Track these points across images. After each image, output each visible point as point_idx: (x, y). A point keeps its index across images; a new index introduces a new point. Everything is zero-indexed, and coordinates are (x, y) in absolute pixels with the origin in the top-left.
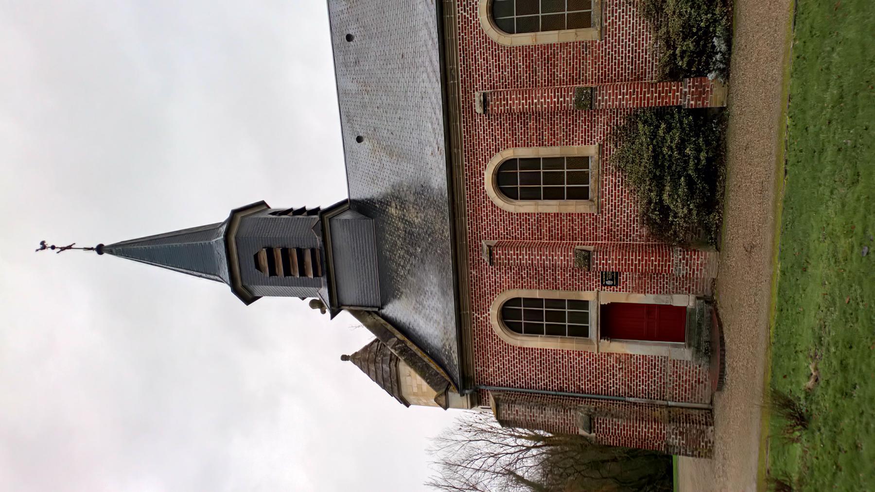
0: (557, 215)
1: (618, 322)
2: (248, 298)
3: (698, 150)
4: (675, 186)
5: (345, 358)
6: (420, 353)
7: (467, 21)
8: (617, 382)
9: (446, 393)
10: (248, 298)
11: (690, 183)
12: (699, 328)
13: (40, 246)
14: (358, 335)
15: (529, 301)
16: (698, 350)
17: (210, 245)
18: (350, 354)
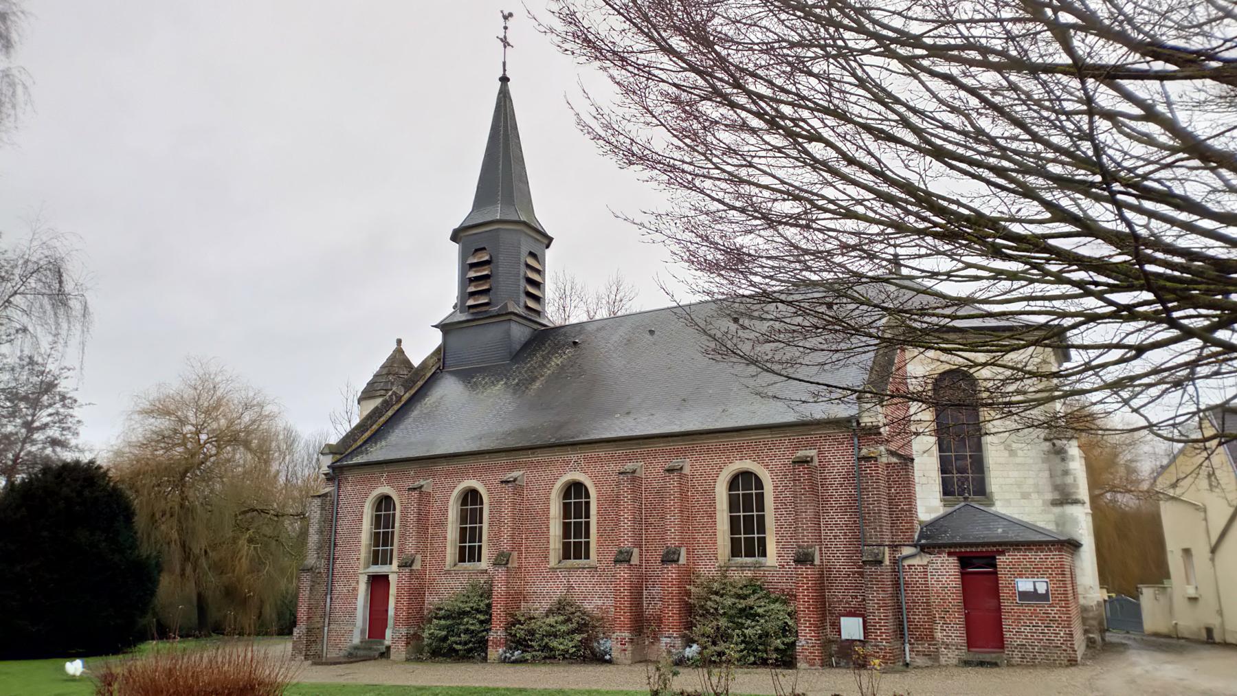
0: (445, 538)
1: (378, 583)
3: (466, 643)
5: (399, 342)
6: (383, 419)
8: (340, 588)
10: (455, 236)
11: (445, 639)
12: (372, 649)
13: (506, 13)
15: (761, 497)
16: (356, 648)
18: (403, 346)
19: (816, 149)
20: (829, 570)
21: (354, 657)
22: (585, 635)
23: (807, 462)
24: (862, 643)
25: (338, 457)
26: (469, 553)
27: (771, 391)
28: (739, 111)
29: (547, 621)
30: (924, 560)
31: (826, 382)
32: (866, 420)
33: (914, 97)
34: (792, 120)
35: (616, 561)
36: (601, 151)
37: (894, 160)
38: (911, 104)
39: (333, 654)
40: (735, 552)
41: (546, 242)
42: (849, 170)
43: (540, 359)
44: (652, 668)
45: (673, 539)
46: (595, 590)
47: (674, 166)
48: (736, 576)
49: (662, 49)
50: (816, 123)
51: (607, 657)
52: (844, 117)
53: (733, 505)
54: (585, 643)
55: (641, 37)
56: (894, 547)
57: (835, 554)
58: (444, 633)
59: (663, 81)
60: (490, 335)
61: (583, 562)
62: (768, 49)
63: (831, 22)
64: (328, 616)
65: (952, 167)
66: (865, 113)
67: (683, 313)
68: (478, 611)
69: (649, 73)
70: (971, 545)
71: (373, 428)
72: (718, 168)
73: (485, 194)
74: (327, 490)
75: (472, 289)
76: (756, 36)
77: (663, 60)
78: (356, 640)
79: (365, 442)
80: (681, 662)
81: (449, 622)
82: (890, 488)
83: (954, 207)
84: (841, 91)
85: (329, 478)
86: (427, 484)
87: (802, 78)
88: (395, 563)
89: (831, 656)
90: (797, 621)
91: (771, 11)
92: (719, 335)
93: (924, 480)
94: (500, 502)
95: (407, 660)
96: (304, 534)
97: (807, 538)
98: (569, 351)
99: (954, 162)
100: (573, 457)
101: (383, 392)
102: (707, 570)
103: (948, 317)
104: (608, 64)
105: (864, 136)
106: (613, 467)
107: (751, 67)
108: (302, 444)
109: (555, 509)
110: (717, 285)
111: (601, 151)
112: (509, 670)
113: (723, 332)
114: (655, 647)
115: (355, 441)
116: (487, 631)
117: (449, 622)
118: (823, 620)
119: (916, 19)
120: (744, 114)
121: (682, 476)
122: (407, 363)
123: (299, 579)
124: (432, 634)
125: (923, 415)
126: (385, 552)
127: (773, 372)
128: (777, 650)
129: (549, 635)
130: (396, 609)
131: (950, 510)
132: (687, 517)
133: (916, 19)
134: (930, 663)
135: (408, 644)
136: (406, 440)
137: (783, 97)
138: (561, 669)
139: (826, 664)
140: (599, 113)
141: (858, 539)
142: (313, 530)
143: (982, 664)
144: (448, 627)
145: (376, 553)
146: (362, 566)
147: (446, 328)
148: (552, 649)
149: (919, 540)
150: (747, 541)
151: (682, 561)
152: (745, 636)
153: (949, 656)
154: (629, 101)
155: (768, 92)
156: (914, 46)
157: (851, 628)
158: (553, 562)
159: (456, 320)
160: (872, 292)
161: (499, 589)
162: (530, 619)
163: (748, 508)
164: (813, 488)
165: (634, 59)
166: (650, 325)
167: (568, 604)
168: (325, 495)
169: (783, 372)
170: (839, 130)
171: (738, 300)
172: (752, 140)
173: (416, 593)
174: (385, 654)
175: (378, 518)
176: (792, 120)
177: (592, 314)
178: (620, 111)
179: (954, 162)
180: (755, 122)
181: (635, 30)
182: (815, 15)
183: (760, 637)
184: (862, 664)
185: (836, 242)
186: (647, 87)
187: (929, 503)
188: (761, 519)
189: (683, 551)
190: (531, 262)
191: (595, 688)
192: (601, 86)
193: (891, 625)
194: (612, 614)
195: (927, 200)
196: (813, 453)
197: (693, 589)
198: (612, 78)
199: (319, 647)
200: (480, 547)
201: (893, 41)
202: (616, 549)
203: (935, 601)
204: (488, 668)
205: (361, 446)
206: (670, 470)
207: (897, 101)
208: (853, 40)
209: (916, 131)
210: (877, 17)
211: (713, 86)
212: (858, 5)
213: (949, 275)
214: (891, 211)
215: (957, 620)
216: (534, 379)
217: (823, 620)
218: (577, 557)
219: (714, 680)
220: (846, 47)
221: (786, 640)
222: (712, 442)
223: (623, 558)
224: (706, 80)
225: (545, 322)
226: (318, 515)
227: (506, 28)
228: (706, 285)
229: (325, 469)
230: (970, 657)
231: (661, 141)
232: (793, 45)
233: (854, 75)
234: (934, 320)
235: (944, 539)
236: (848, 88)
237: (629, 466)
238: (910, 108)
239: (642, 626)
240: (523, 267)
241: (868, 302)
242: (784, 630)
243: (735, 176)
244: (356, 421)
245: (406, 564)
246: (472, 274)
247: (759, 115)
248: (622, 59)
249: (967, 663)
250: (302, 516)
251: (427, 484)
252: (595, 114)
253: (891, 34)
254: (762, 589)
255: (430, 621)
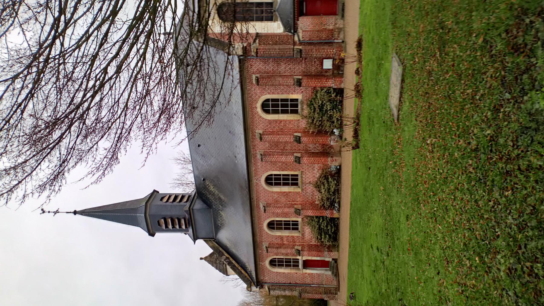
1: (307, 264)
2: (152, 235)
3: (332, 227)
4: (325, 237)
5: (201, 259)
6: (236, 265)
7: (257, 183)
8: (308, 281)
9: (251, 287)
10: (152, 235)
11: (330, 236)
12: (333, 266)
13: (42, 212)
14: (204, 248)
15: (273, 100)
16: (333, 273)
17: (136, 216)
19: (111, 70)
20: (304, 72)
21: (336, 274)
22: (329, 176)
23: (258, 79)
24: (334, 60)
25: (252, 284)
26: (295, 226)
27: (227, 96)
28: (91, 106)
29: (323, 192)
30: (300, 31)
31: (223, 70)
32: (240, 52)
33: (86, 23)
34: (96, 81)
35: (299, 163)
36: (110, 173)
37: (116, 35)
38: (89, 25)
39: (335, 283)
40: (296, 112)
41: (156, 193)
42: (122, 55)
43: (210, 196)
44: (343, 149)
45: (289, 139)
46: (310, 172)
47: (119, 137)
48: (306, 112)
49: (59, 141)
50: (98, 71)
51: (338, 167)
52: (95, 57)
53: (276, 112)
54: (332, 176)
55: (53, 152)
56: (294, 44)
57: (298, 69)
58: (327, 236)
59: (75, 142)
60: (199, 218)
61: (299, 177)
62: (60, 91)
63: (46, 61)
64: (319, 285)
65: (121, 7)
66: (94, 46)
67: (191, 135)
68: (319, 222)
69: (71, 149)
70: (294, 11)
71: (240, 268)
72: (119, 117)
73: (131, 221)
74: (266, 288)
75: (177, 227)
76: (53, 97)
77: (64, 143)
78: (330, 273)
79: (247, 272)
80: (341, 137)
81: (323, 234)
82: (269, 44)
83: (140, 9)
84: (82, 57)
85: (262, 287)
86: (265, 245)
87: (75, 75)
88: (298, 257)
89: (339, 74)
90: (325, 87)
91: (40, 89)
92: (202, 119)
93: (266, 29)
94: (273, 213)
95: (338, 251)
96: (285, 297)
97: (291, 81)
98: (207, 183)
99: (119, 6)
100: (254, 181)
101: (224, 265)
102: (303, 124)
103: (193, 14)
104: (66, 169)
105: (106, 47)
106: (259, 164)
107: (69, 100)
108: (246, 299)
109: (276, 189)
110: (178, 118)
111: (110, 173)
112: (342, 209)
113: (199, 113)
114: (334, 147)
115: (246, 277)
116: (327, 217)
117: (323, 234)
118: (324, 76)
119: (45, 20)
120: (93, 104)
121: (263, 134)
122: (211, 255)
123: (304, 299)
124: (328, 241)
125: (240, 27)
126: (293, 262)
127: (219, 95)
128: (336, 96)
129: (329, 192)
130: (317, 256)
131: (279, 19)
132: (281, 132)
133: (45, 20)
134: (342, 32)
135: (331, 251)
136: (246, 255)
137: (84, 86)
138: (343, 187)
139: (342, 76)
140: (92, 173)
141: (291, 59)
142: (283, 293)
143: (343, 10)
144: (325, 235)
145: (294, 266)
146: (299, 272)
147: (195, 238)
148: (335, 190)
149: (291, 33)
150: (290, 106)
151: (299, 135)
152: (330, 110)
153: (340, 23)
154: (85, 158)
155: (81, 94)
156: (59, 21)
157: (328, 64)
158: (299, 190)
159: (192, 234)
160: (181, 48)
161: (310, 213)
162: (322, 200)
163: (277, 106)
164: (269, 77)
165: (64, 157)
166: (196, 146)
167: (317, 184)
168: (269, 289)
169: (219, 90)
170: (102, 58)
171: (185, 109)
172: (106, 100)
173: (311, 248)
174: (335, 260)
175: (279, 265)
176: (96, 81)
177: (190, 171)
178: (90, 163)
179: (119, 6)
180: (97, 98)
181: (49, 156)
182: (43, 68)
183: (331, 103)
184: (343, 60)
185: (158, 64)
186: (78, 150)
187: (275, 27)
188: (282, 100)
189: (296, 134)
190: (165, 200)
191: (350, 173)
192: (77, 173)
193: (326, 47)
194: (322, 166)
195: (138, 19)
196: (254, 77)
197: (311, 131)
198: (73, 167)
199: (332, 289)
200: (292, 221)
201: (56, 31)
202: (295, 163)
203: (317, 28)
204: (342, 217)
205: (248, 274)
206: (261, 139)
207: (88, 31)
208: (56, 51)
209: (103, 22)
210: (44, 39)
211: (79, 119)
212: (38, 47)
213: (174, 12)
214: (142, 38)
215: (325, 18)
216: (220, 199)
217: (324, 76)
218: (297, 179)
219: (348, 123)
220: (59, 55)
221: (332, 92)
222: (249, 121)
223: (298, 160)
224: (76, 121)
225: (193, 193)
226: (277, 292)
227: (49, 212)
228: (178, 124)
229: (258, 289)
230: (340, 14)
231: (105, 144)
232: (58, 79)
233: (74, 50)
234: (195, 20)
235: (291, 22)
236: (81, 54)
237: (259, 157)
238: (92, 24)
239: (326, 152)
240: (167, 203)
241: (186, 50)
242: (328, 93)
243: (124, 109)
244: (237, 276)
245: (299, 253)
246: (170, 227)
247: (93, 97)
248: (64, 162)
249: (343, 16)
250: (278, 297)
251: (265, 245)
252: (91, 175)
253: (53, 32)
254: (311, 101)
255: (322, 242)
